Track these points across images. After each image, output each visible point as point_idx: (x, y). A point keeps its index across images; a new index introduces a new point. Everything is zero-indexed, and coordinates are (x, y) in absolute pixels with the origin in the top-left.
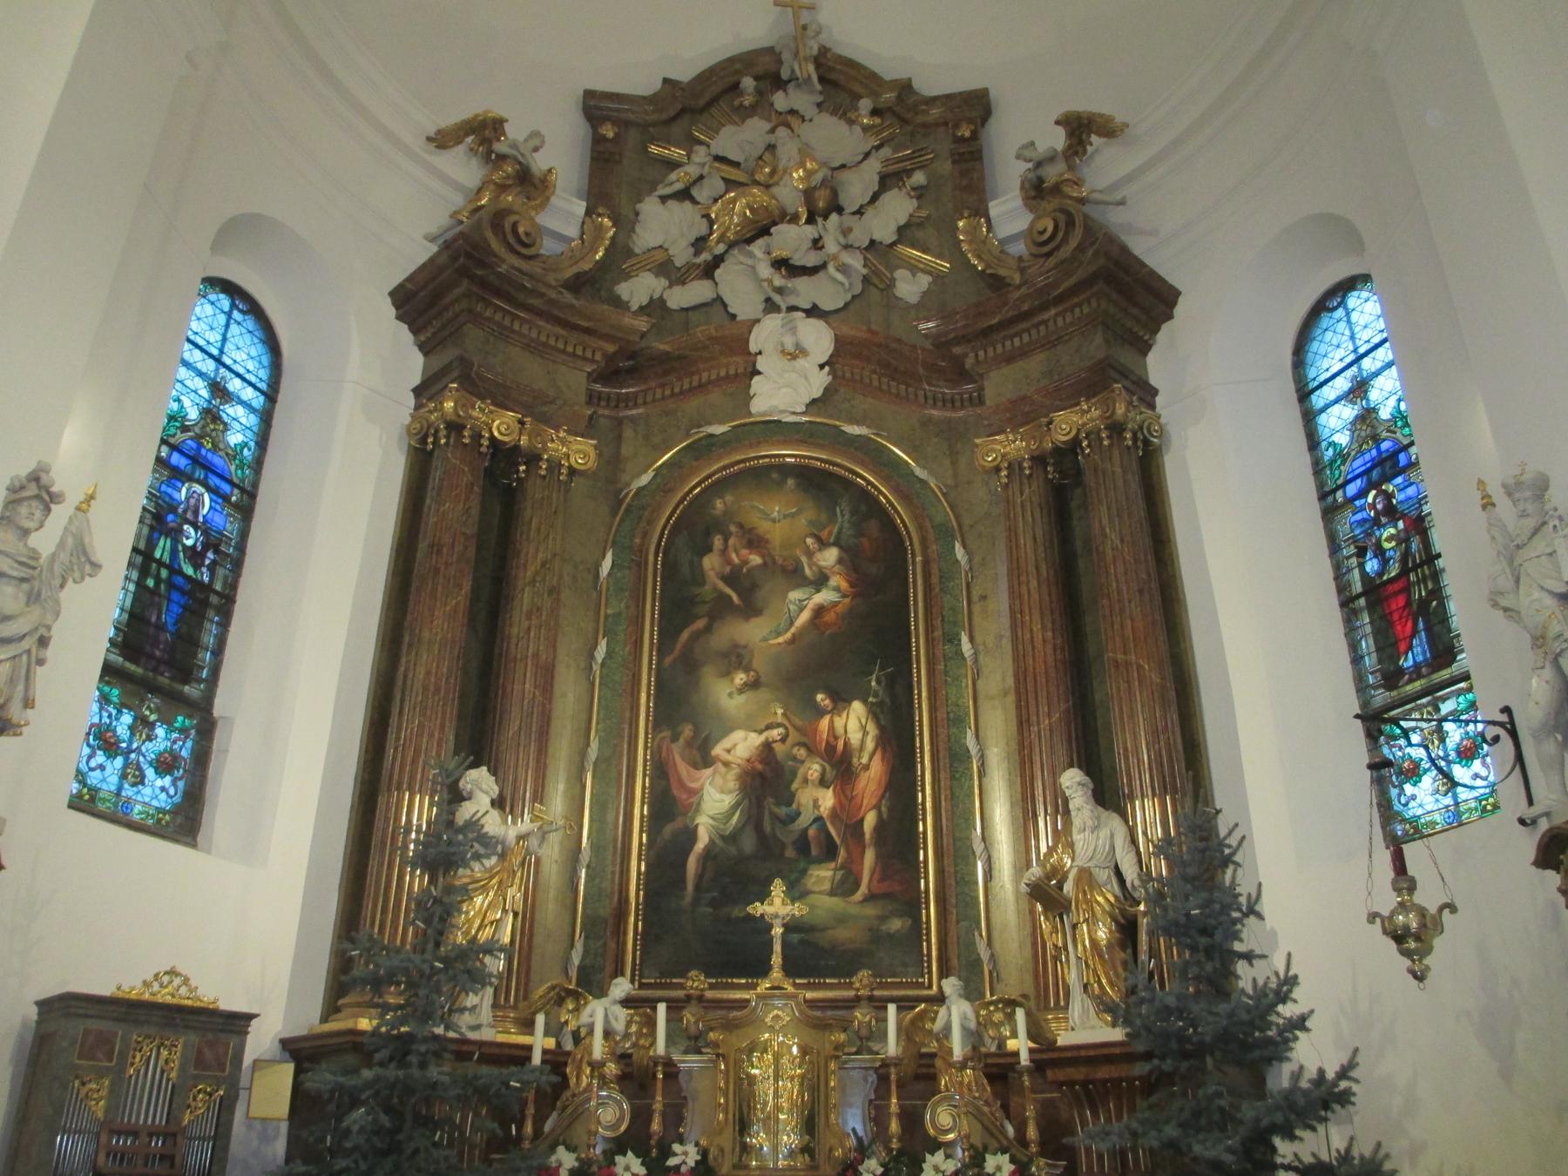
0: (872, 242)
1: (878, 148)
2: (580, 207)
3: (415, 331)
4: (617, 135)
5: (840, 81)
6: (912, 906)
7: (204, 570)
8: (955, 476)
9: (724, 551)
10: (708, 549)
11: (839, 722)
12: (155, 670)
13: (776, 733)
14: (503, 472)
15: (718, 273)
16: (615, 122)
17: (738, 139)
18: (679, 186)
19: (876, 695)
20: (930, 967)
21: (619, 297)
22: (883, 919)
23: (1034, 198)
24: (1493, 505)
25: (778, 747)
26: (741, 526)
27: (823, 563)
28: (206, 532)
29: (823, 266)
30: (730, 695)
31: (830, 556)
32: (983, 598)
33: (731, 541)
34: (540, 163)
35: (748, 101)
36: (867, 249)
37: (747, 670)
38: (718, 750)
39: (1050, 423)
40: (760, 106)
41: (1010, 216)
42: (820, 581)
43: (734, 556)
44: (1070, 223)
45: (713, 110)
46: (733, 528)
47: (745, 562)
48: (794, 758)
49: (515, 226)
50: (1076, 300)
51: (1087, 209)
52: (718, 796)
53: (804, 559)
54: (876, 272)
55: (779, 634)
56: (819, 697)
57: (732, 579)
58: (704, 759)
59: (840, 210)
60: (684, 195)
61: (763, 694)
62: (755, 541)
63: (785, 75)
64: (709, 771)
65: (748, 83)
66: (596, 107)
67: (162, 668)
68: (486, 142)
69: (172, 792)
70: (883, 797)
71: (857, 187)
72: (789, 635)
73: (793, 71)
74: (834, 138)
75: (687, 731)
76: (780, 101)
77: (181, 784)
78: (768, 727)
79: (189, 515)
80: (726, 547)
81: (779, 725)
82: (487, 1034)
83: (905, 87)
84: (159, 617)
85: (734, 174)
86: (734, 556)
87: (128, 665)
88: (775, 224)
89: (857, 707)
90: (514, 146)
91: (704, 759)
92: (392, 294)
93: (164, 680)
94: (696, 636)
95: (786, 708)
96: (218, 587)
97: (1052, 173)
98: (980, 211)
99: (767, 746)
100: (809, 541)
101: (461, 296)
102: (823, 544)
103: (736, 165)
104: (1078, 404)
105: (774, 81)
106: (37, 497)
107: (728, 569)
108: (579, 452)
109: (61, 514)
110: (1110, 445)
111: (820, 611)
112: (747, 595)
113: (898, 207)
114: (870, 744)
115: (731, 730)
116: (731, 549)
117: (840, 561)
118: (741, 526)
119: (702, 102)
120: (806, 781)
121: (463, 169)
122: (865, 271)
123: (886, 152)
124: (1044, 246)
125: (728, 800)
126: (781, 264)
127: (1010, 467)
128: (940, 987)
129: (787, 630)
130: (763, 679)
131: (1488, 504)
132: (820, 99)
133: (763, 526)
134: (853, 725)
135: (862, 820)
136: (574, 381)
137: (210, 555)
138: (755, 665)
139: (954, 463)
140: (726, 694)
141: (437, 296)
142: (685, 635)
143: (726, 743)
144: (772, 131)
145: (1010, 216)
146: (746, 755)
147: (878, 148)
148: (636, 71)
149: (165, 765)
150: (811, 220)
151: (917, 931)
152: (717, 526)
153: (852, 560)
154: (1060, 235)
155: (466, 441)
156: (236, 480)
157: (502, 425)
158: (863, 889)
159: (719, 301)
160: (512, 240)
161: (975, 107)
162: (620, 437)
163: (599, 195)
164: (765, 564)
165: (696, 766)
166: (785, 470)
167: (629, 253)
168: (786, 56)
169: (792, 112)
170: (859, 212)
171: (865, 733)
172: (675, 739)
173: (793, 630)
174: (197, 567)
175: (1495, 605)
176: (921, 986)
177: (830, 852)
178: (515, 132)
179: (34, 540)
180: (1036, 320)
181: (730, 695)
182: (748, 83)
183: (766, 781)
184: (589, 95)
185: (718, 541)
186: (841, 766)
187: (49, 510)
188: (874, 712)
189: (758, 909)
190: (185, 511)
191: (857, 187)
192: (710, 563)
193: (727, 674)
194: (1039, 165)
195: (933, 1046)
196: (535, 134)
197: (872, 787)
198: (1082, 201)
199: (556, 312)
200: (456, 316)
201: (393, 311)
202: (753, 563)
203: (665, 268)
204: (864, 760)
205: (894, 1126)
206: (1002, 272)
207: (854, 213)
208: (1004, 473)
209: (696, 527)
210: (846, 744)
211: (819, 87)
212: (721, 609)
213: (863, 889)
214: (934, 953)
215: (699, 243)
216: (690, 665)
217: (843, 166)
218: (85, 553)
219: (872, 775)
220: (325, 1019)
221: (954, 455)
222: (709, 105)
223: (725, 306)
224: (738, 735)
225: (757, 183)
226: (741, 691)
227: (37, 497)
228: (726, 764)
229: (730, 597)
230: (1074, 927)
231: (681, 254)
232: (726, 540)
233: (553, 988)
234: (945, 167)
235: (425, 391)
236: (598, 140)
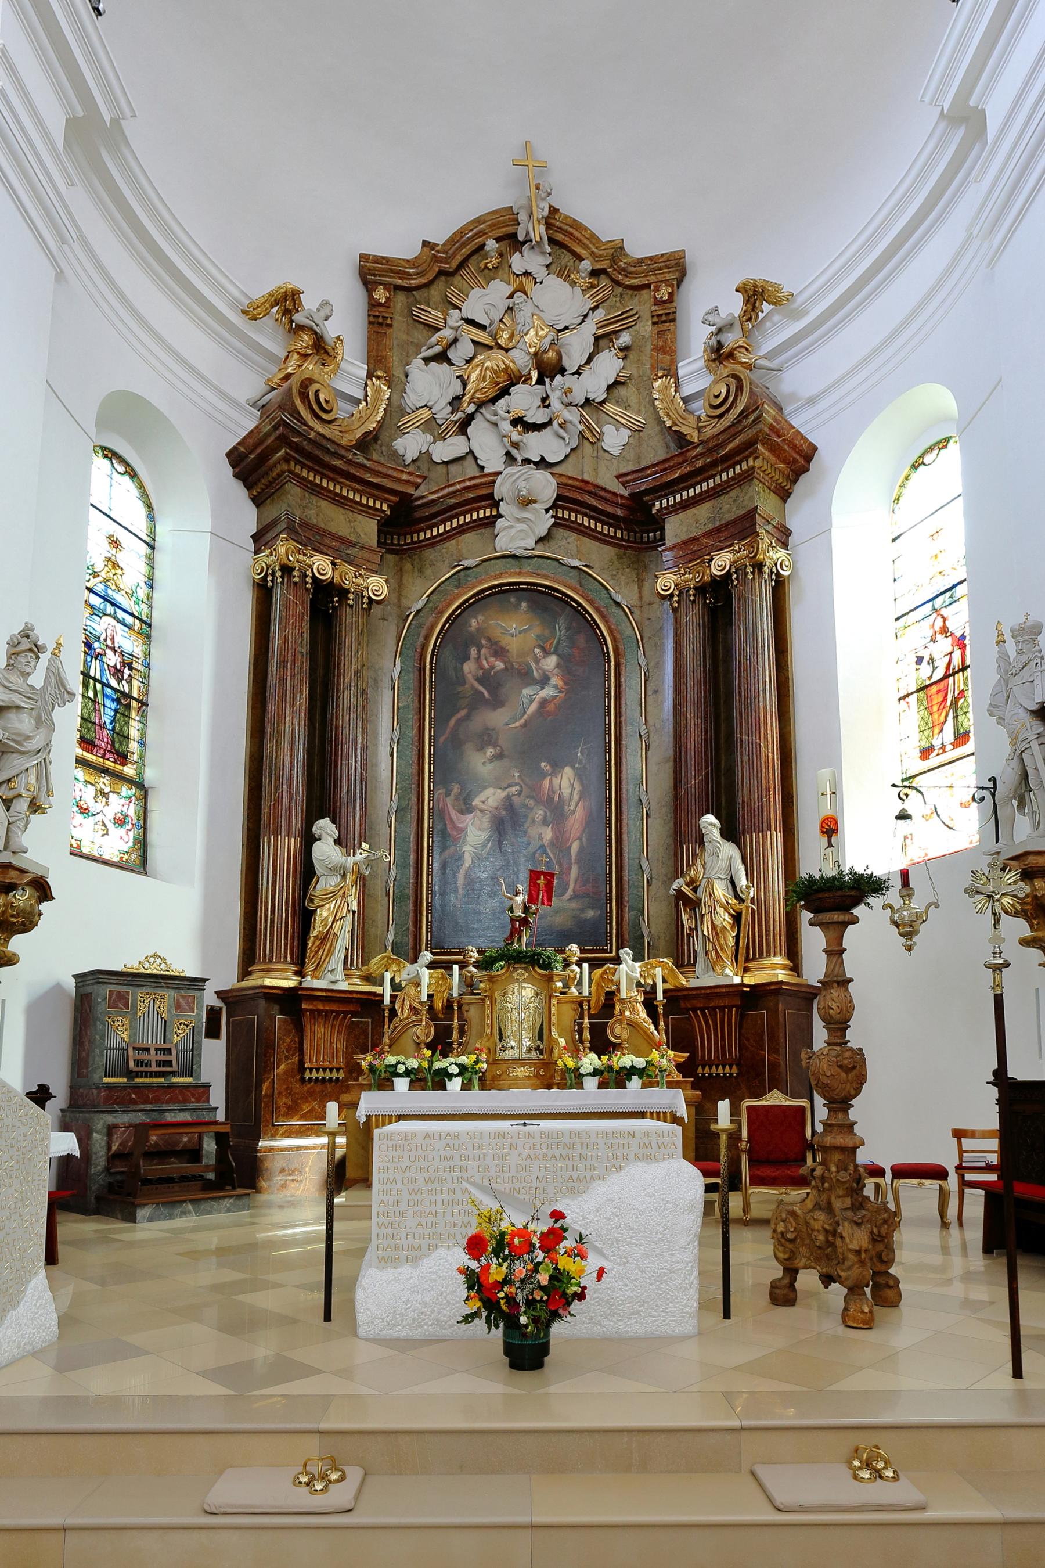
0: (587, 400)
1: (593, 309)
2: (362, 371)
3: (249, 487)
4: (388, 299)
5: (564, 239)
7: (124, 682)
8: (641, 598)
9: (478, 659)
10: (467, 658)
11: (556, 781)
12: (103, 757)
13: (514, 790)
14: (325, 602)
15: (470, 430)
16: (387, 286)
17: (484, 300)
18: (438, 349)
19: (580, 762)
20: (611, 940)
21: (396, 451)
22: (583, 910)
23: (714, 360)
24: (1004, 642)
25: (516, 800)
26: (489, 639)
27: (546, 667)
28: (122, 654)
29: (549, 423)
30: (484, 763)
31: (551, 662)
32: (656, 691)
33: (483, 651)
34: (331, 330)
35: (492, 262)
36: (582, 406)
37: (495, 745)
38: (476, 802)
39: (711, 560)
41: (695, 375)
42: (544, 681)
43: (484, 662)
44: (740, 388)
45: (463, 272)
46: (483, 642)
47: (493, 667)
48: (526, 806)
49: (317, 392)
50: (737, 459)
51: (754, 375)
52: (478, 833)
53: (533, 665)
54: (589, 428)
55: (516, 721)
56: (543, 764)
57: (485, 679)
58: (467, 808)
59: (562, 371)
60: (442, 357)
61: (505, 762)
62: (499, 652)
63: (521, 238)
64: (471, 816)
65: (491, 245)
66: (372, 272)
67: (108, 755)
68: (287, 312)
69: (126, 838)
70: (584, 831)
71: (577, 346)
72: (522, 721)
73: (528, 233)
75: (456, 789)
76: (518, 262)
77: (131, 833)
78: (510, 786)
79: (109, 643)
80: (479, 657)
81: (516, 784)
82: (343, 986)
83: (618, 249)
84: (100, 719)
85: (483, 337)
86: (484, 662)
87: (85, 754)
88: (513, 384)
89: (568, 771)
90: (310, 317)
91: (467, 808)
92: (228, 455)
93: (110, 764)
94: (459, 722)
95: (521, 772)
96: (135, 694)
97: (730, 339)
98: (671, 372)
99: (508, 798)
100: (537, 650)
101: (281, 459)
102: (546, 653)
103: (483, 328)
104: (732, 545)
105: (513, 242)
106: (30, 650)
107: (481, 672)
108: (377, 585)
109: (45, 657)
110: (754, 578)
111: (544, 702)
113: (608, 366)
114: (576, 797)
115: (485, 788)
116: (482, 657)
117: (558, 666)
118: (489, 639)
119: (455, 264)
120: (534, 821)
121: (269, 337)
122: (581, 427)
123: (600, 314)
124: (719, 407)
125: (483, 836)
126: (517, 422)
127: (681, 593)
128: (618, 954)
129: (521, 718)
130: (506, 753)
131: (1000, 642)
132: (549, 260)
133: (507, 642)
134: (565, 784)
135: (570, 848)
136: (368, 530)
137: (127, 672)
138: (500, 742)
139: (640, 588)
140: (480, 763)
141: (263, 458)
142: (452, 722)
143: (482, 796)
144: (511, 296)
145: (695, 375)
146: (495, 805)
147: (593, 309)
148: (400, 242)
149: (121, 821)
150: (540, 381)
152: (472, 640)
154: (731, 399)
155: (296, 579)
156: (136, 614)
157: (321, 565)
158: (570, 892)
160: (315, 407)
161: (674, 268)
162: (401, 570)
163: (377, 361)
164: (506, 669)
165: (461, 812)
166: (514, 588)
167: (403, 413)
168: (523, 217)
169: (527, 274)
170: (578, 373)
171: (573, 789)
172: (448, 794)
173: (525, 717)
174: (119, 681)
175: (906, 838)
176: (606, 951)
178: (309, 302)
179: (31, 681)
180: (706, 475)
181: (484, 763)
182: (491, 245)
184: (363, 257)
185: (473, 652)
186: (557, 811)
187: (38, 658)
188: (580, 775)
190: (105, 640)
192: (469, 667)
193: (481, 749)
194: (720, 331)
195: (763, 1198)
196: (326, 303)
197: (577, 825)
198: (750, 367)
199: (352, 471)
200: (279, 475)
201: (230, 471)
202: (498, 668)
203: (431, 425)
204: (572, 808)
205: (587, 1035)
206: (685, 430)
207: (573, 374)
208: (676, 599)
209: (456, 636)
210: (560, 796)
211: (548, 249)
212: (477, 702)
213: (570, 892)
214: (614, 931)
215: (456, 402)
216: (457, 742)
217: (566, 328)
218: (63, 686)
220: (241, 979)
221: (640, 582)
222: (462, 265)
223: (476, 459)
224: (489, 791)
225: (500, 347)
226: (491, 761)
227: (30, 650)
228: (482, 811)
229: (482, 693)
230: (702, 916)
231: (442, 411)
232: (479, 652)
233: (383, 958)
234: (646, 328)
235: (261, 539)
236: (373, 304)
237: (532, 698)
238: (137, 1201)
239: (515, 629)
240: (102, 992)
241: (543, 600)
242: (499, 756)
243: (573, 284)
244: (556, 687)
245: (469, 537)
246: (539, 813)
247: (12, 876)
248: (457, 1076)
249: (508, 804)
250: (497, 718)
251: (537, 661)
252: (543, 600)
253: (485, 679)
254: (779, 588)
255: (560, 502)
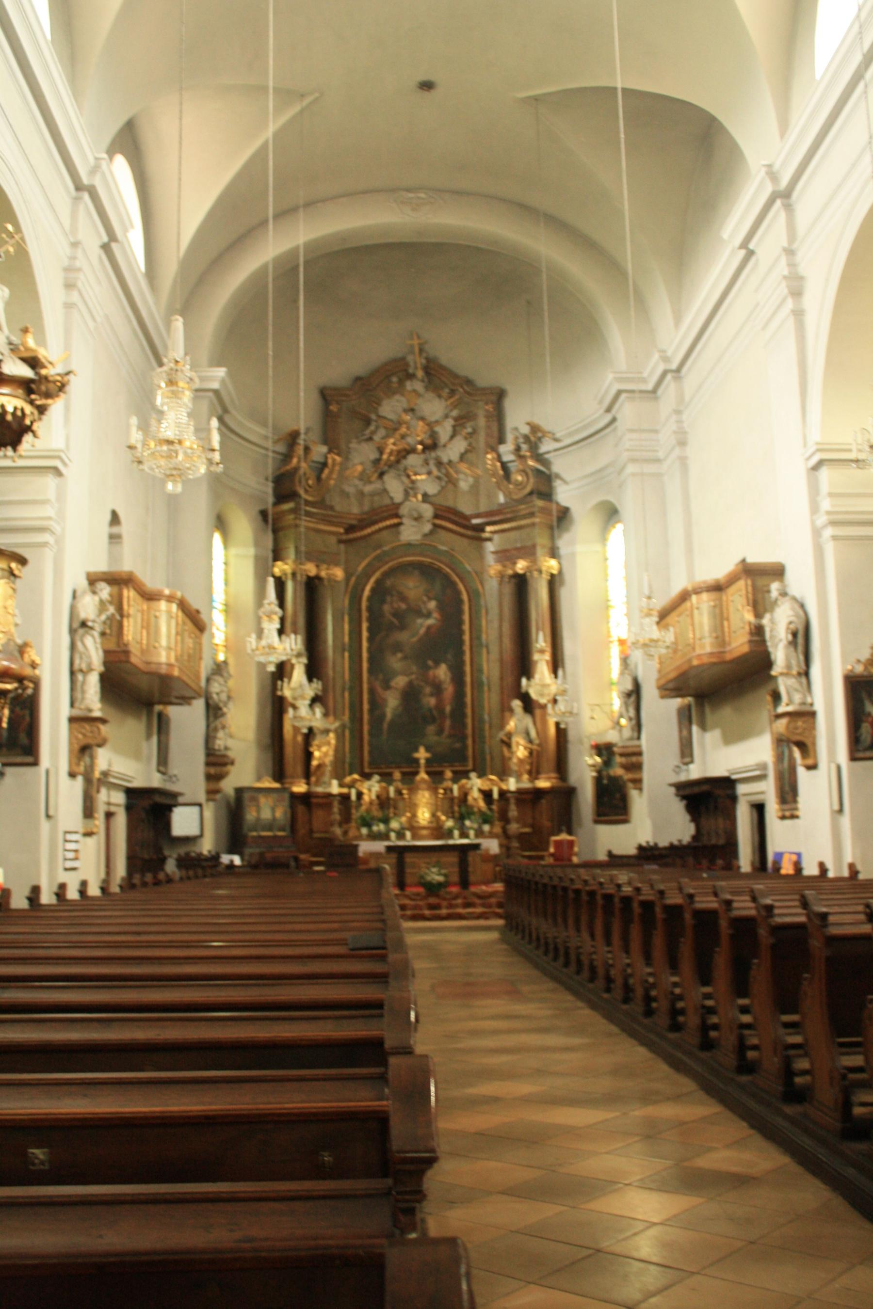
6: (463, 738)
13: (413, 677)
31: (432, 605)
37: (401, 651)
40: (400, 389)
42: (428, 615)
60: (370, 439)
62: (403, 598)
74: (434, 407)
75: (381, 676)
76: (409, 385)
91: (387, 687)
102: (430, 599)
111: (429, 628)
112: (402, 620)
113: (459, 446)
140: (395, 662)
151: (465, 747)
153: (441, 607)
159: (385, 491)
166: (412, 565)
177: (434, 720)
183: (410, 695)
185: (389, 599)
186: (438, 689)
188: (451, 668)
189: (416, 755)
191: (444, 431)
192: (386, 608)
193: (394, 653)
212: (391, 628)
219: (449, 690)
237: (423, 624)
238: (516, 795)
239: (413, 587)
240: (246, 795)
241: (427, 571)
242: (405, 658)
243: (440, 396)
244: (436, 619)
245: (385, 533)
246: (428, 690)
247: (226, 760)
248: (393, 830)
249: (410, 684)
250: (403, 637)
251: (424, 603)
252: (427, 571)
253: (397, 614)
254: (554, 583)
255: (436, 516)
